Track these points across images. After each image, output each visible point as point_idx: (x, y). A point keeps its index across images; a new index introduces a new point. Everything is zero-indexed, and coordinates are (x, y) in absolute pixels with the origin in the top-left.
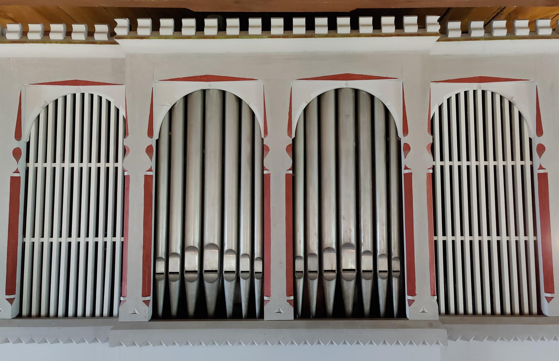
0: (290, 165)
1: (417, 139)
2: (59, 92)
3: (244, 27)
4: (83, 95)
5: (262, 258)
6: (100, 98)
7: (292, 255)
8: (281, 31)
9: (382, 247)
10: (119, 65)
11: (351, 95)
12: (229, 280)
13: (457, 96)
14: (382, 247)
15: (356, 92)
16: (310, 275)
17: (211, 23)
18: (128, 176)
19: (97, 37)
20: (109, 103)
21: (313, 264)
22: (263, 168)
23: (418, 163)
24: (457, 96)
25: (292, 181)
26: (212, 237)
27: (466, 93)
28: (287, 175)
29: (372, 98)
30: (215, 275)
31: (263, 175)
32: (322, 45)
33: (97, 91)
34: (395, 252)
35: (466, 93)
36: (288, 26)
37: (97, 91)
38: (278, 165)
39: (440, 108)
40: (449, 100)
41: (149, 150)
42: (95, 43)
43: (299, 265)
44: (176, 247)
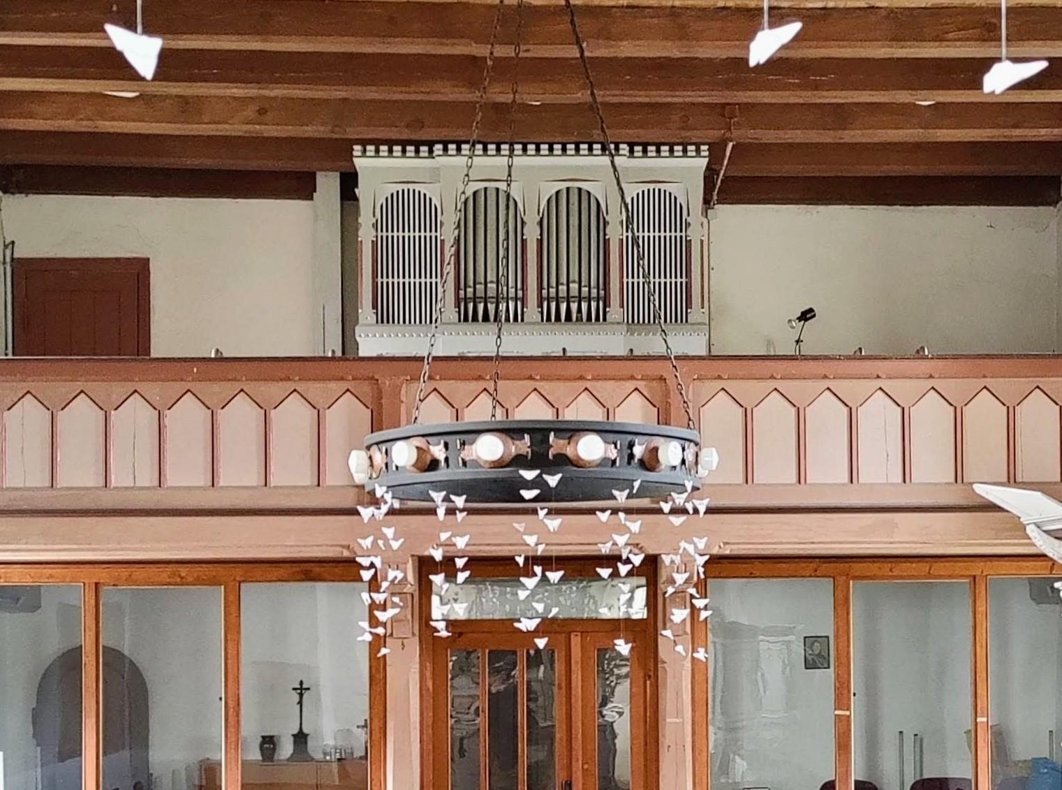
0: (539, 232)
1: (615, 217)
2: (400, 187)
3: (645, 151)
4: (409, 190)
5: (605, 289)
6: (419, 192)
7: (540, 288)
8: (533, 153)
9: (593, 283)
10: (436, 171)
11: (576, 192)
12: (492, 303)
13: (643, 192)
14: (593, 283)
15: (580, 190)
16: (477, 300)
17: (397, 148)
18: (526, 240)
19: (368, 154)
20: (425, 195)
21: (553, 291)
22: (523, 235)
23: (615, 232)
24: (398, 192)
25: (540, 242)
26: (574, 275)
27: (403, 191)
28: (538, 239)
29: (589, 193)
30: (494, 300)
31: (522, 239)
32: (558, 161)
33: (417, 187)
34: (601, 286)
35: (649, 190)
36: (591, 149)
37: (417, 187)
38: (532, 233)
39: (633, 199)
40: (638, 194)
41: (373, 224)
42: (634, 157)
43: (545, 292)
44: (564, 279)
